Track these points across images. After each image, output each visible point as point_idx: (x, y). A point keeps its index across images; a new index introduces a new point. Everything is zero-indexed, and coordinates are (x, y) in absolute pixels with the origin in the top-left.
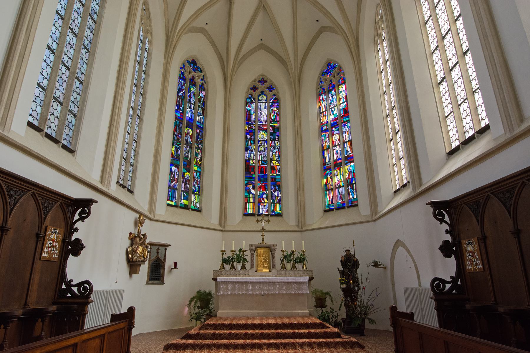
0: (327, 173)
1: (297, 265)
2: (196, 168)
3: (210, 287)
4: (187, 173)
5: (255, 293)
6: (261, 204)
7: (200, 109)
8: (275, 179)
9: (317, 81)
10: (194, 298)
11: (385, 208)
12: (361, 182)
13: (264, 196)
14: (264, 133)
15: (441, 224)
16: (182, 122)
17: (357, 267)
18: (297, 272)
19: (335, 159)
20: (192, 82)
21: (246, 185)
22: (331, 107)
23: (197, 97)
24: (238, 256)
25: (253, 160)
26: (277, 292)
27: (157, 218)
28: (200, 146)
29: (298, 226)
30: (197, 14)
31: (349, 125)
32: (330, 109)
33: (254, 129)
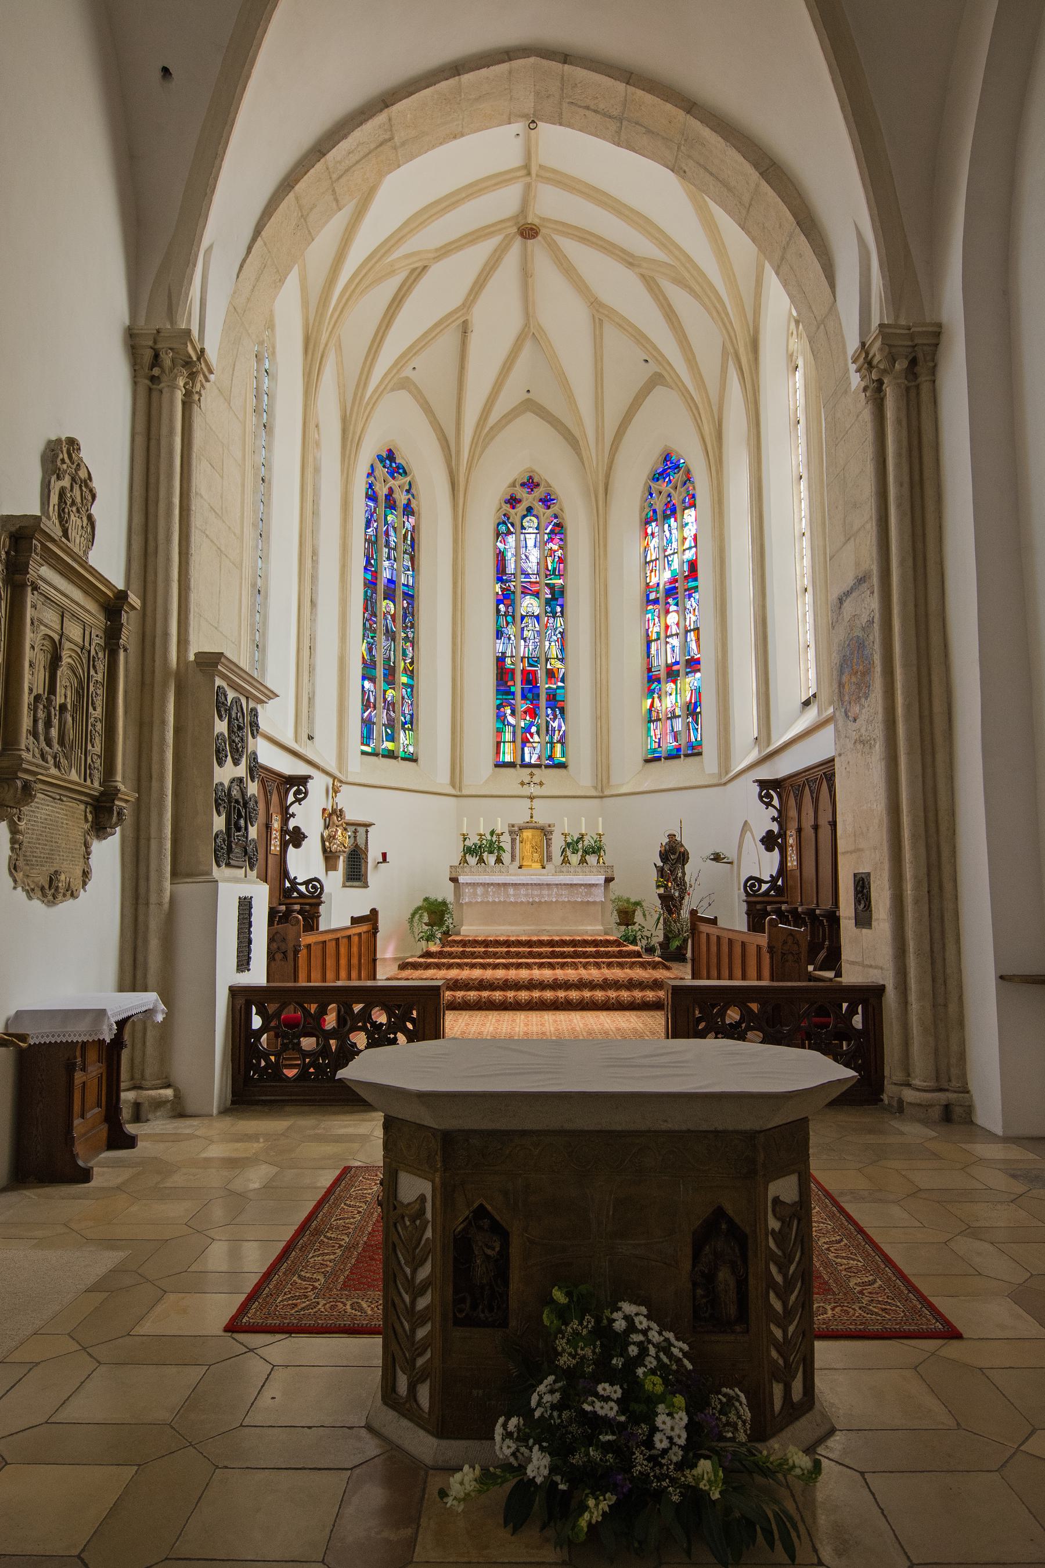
0: (652, 687)
1: (587, 857)
2: (404, 679)
3: (445, 892)
4: (390, 691)
5: (519, 900)
6: (528, 744)
7: (406, 556)
8: (555, 696)
9: (643, 492)
10: (419, 908)
11: (778, 740)
12: (708, 710)
13: (534, 729)
14: (532, 601)
15: (767, 808)
16: (376, 590)
17: (683, 860)
18: (587, 869)
19: (669, 662)
20: (391, 503)
21: (499, 707)
22: (667, 554)
23: (401, 532)
24: (491, 843)
25: (512, 656)
26: (554, 900)
27: (350, 779)
28: (410, 635)
29: (596, 788)
30: (399, 366)
31: (696, 595)
32: (665, 556)
33: (514, 592)
